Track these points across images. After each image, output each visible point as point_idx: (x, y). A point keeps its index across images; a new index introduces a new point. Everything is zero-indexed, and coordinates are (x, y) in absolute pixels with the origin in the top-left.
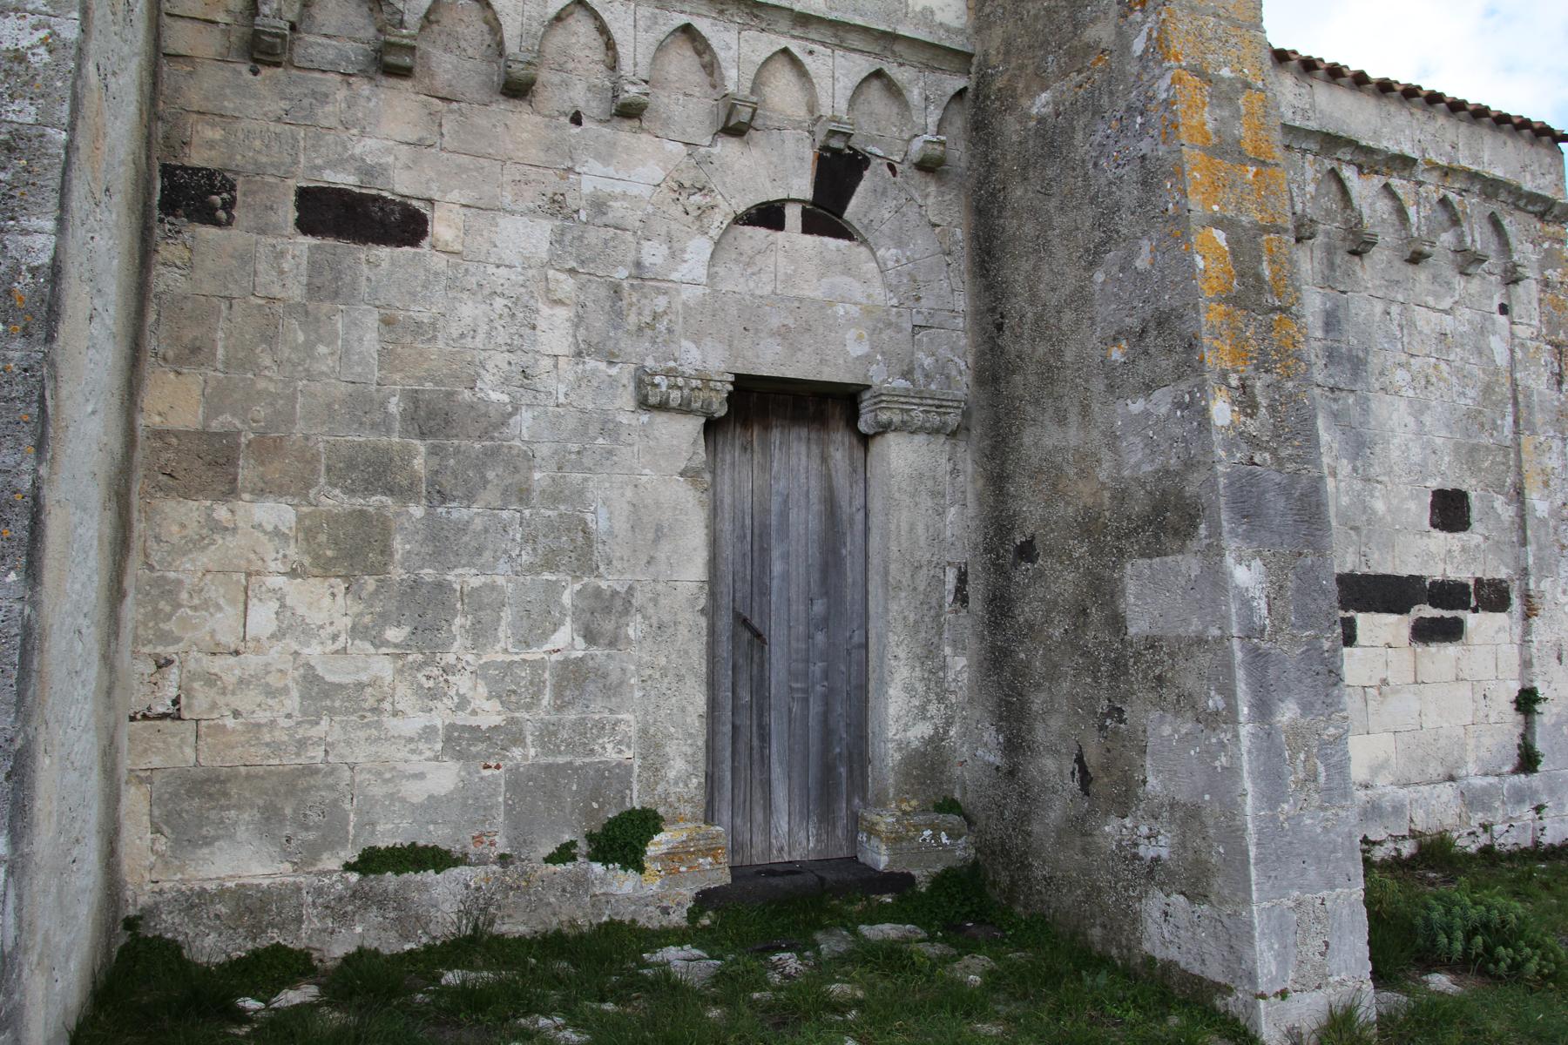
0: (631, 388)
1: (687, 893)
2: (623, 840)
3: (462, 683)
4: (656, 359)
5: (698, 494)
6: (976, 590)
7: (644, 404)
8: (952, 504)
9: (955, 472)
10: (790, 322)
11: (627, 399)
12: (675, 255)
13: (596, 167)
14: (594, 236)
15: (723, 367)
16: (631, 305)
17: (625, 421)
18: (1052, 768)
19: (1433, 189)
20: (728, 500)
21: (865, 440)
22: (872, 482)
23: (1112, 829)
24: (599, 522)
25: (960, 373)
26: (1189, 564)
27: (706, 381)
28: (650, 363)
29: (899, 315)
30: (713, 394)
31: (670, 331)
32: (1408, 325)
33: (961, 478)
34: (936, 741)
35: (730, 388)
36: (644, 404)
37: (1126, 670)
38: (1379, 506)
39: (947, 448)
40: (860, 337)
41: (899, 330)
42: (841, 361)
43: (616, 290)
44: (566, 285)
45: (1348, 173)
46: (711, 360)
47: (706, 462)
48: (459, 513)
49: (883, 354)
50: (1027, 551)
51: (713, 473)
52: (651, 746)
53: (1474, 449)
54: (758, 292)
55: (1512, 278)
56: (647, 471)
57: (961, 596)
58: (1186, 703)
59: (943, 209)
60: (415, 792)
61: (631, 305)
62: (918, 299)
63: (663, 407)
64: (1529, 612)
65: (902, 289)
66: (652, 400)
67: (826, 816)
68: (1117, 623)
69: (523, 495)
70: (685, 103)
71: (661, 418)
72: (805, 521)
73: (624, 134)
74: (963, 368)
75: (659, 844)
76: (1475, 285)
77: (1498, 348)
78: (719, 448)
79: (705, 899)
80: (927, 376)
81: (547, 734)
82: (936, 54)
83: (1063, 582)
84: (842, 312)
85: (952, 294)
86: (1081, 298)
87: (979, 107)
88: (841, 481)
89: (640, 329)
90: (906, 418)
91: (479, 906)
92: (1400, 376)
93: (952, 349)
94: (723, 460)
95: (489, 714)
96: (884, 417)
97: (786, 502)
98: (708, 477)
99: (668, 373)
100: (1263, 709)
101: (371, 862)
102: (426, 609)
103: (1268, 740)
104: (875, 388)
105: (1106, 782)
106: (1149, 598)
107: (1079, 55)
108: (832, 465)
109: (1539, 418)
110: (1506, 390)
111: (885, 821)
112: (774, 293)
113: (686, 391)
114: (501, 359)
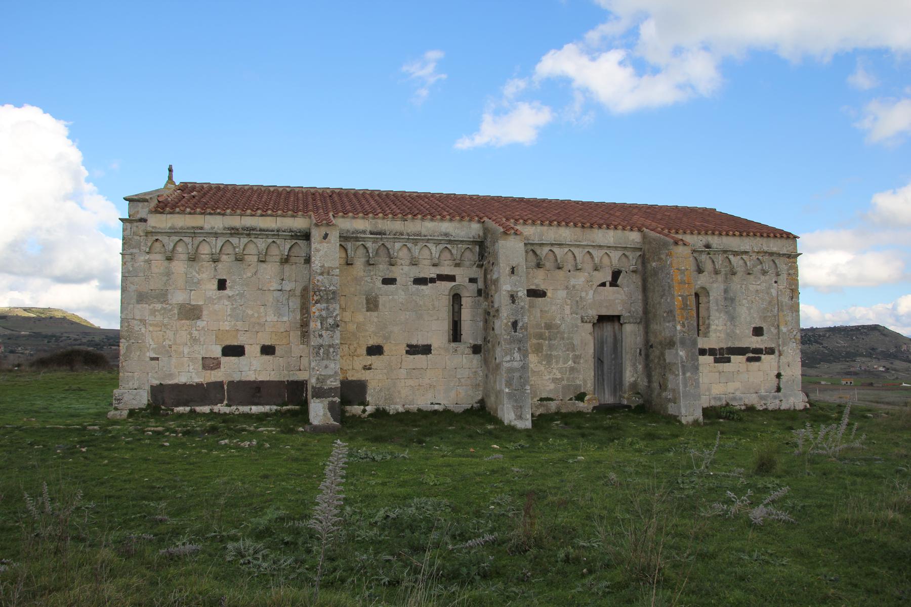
1: (591, 407)
2: (581, 397)
3: (554, 371)
6: (643, 353)
7: (583, 322)
11: (580, 321)
12: (587, 294)
18: (655, 385)
19: (754, 257)
21: (622, 324)
23: (664, 394)
24: (575, 343)
26: (673, 351)
32: (747, 289)
34: (635, 381)
36: (583, 322)
37: (666, 367)
38: (738, 332)
44: (569, 302)
45: (731, 257)
46: (593, 313)
48: (553, 342)
50: (651, 346)
52: (585, 381)
53: (765, 317)
55: (778, 275)
57: (640, 354)
58: (673, 373)
59: (637, 279)
60: (548, 388)
64: (780, 355)
67: (615, 396)
68: (665, 360)
69: (563, 339)
70: (588, 266)
72: (610, 340)
73: (578, 273)
75: (587, 398)
76: (767, 277)
77: (774, 292)
79: (594, 408)
81: (568, 379)
82: (635, 249)
83: (657, 353)
85: (639, 296)
86: (660, 303)
87: (644, 260)
91: (558, 408)
92: (744, 301)
95: (559, 376)
100: (684, 374)
101: (541, 400)
102: (549, 358)
103: (685, 379)
105: (663, 387)
106: (669, 356)
107: (660, 259)
109: (785, 308)
110: (776, 302)
111: (626, 396)
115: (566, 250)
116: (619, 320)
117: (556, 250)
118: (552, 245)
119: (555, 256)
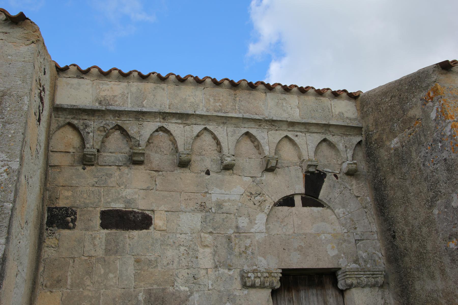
0: (239, 279)
4: (248, 266)
7: (245, 286)
10: (302, 244)
11: (237, 284)
12: (252, 222)
13: (218, 190)
14: (218, 218)
15: (277, 267)
21: (342, 292)
25: (380, 258)
27: (270, 273)
28: (246, 268)
29: (348, 236)
30: (274, 279)
31: (253, 253)
35: (281, 275)
36: (245, 286)
41: (350, 243)
42: (326, 259)
43: (229, 239)
44: (209, 239)
46: (271, 264)
49: (344, 253)
54: (287, 233)
59: (360, 189)
61: (236, 244)
62: (356, 228)
63: (253, 286)
65: (348, 225)
66: (248, 284)
70: (250, 162)
71: (253, 291)
74: (381, 256)
80: (365, 261)
84: (324, 238)
85: (370, 225)
86: (429, 221)
89: (240, 254)
90: (359, 281)
93: (374, 248)
96: (349, 281)
99: (254, 271)
104: (343, 269)
107: (407, 122)
113: (262, 279)
114: (184, 272)
115: (198, 129)
116: (335, 283)
117: (174, 127)
118: (165, 115)
119: (174, 142)
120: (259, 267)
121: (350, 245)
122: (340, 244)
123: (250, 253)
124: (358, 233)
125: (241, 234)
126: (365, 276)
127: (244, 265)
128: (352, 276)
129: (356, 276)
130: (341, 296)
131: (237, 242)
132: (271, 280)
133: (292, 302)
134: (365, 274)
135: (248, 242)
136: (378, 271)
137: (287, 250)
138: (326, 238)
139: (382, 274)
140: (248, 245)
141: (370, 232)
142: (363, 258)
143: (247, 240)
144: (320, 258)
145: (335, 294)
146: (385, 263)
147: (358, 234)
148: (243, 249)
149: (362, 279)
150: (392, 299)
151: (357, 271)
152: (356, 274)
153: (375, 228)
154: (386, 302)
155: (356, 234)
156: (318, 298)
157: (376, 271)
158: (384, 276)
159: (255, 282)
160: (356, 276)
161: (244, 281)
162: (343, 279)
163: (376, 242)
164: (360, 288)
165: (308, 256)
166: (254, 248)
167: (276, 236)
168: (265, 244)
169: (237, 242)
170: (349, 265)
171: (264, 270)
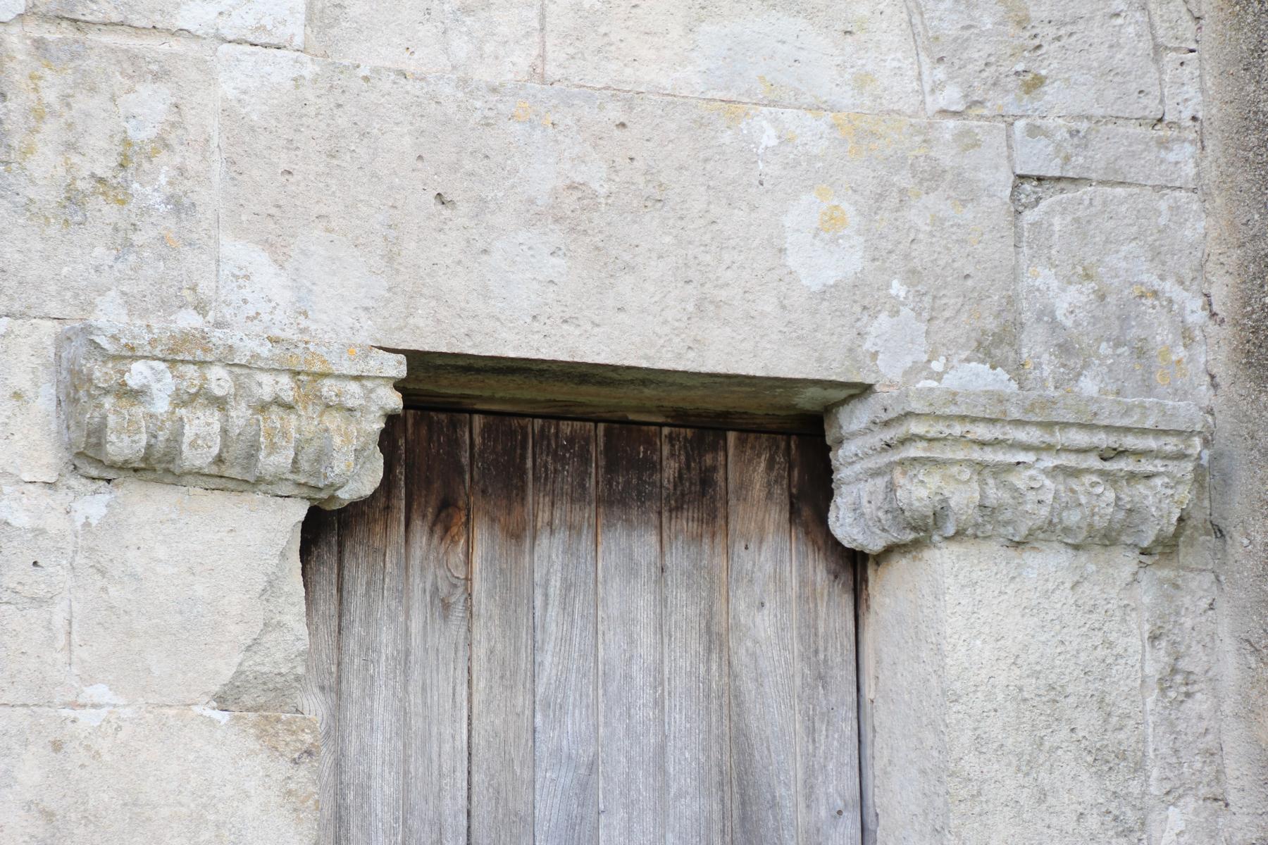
0: (44, 400)
4: (131, 304)
5: (282, 768)
8: (1171, 796)
9: (1175, 680)
10: (595, 175)
15: (368, 331)
16: (39, 114)
17: (21, 519)
20: (384, 787)
21: (855, 567)
22: (880, 717)
25: (1186, 335)
27: (308, 377)
28: (110, 317)
29: (968, 142)
30: (333, 421)
31: (179, 206)
33: (1200, 704)
35: (394, 401)
36: (90, 459)
39: (1146, 595)
40: (832, 221)
41: (967, 193)
42: (768, 305)
46: (334, 314)
47: (308, 656)
49: (912, 276)
51: (335, 690)
54: (483, 74)
56: (99, 692)
61: (39, 114)
62: (1034, 84)
63: (157, 466)
65: (978, 52)
66: (120, 446)
71: (149, 505)
74: (1195, 314)
78: (356, 604)
80: (1065, 349)
84: (769, 138)
88: (774, 712)
89: (73, 199)
90: (995, 494)
93: (1156, 254)
94: (368, 648)
96: (918, 492)
97: (585, 788)
98: (315, 706)
99: (174, 354)
104: (884, 394)
108: (741, 657)
112: (537, 74)
113: (240, 414)
116: (811, 492)
120: (219, 325)
121: (968, 214)
122: (893, 200)
123: (156, 199)
124: (1050, 123)
125: (93, 37)
126: (1049, 461)
127: (102, 291)
128: (949, 454)
129: (977, 454)
130: (847, 601)
131: (50, 96)
132: (310, 428)
133: (458, 612)
134: (1049, 448)
135: (148, 108)
136: (1158, 432)
137: (463, 208)
138: (784, 140)
139: (1181, 456)
140: (143, 134)
141: (1141, 121)
142: (1054, 325)
143: (145, 90)
144: (723, 294)
145: (803, 582)
146: (1218, 370)
147: (1047, 134)
148: (104, 166)
149: (1020, 480)
150: (1228, 645)
151: (992, 421)
152: (983, 444)
153: (1191, 90)
154: (1183, 664)
155: (1033, 131)
156: (664, 601)
157: (1144, 432)
158: (1198, 468)
159: (176, 437)
160: (977, 454)
161: (91, 416)
162: (876, 473)
163: (1175, 209)
164: (993, 547)
165: (628, 268)
166: (193, 163)
167: (386, 85)
168: (290, 145)
169: (50, 96)
170: (937, 366)
171: (265, 350)
